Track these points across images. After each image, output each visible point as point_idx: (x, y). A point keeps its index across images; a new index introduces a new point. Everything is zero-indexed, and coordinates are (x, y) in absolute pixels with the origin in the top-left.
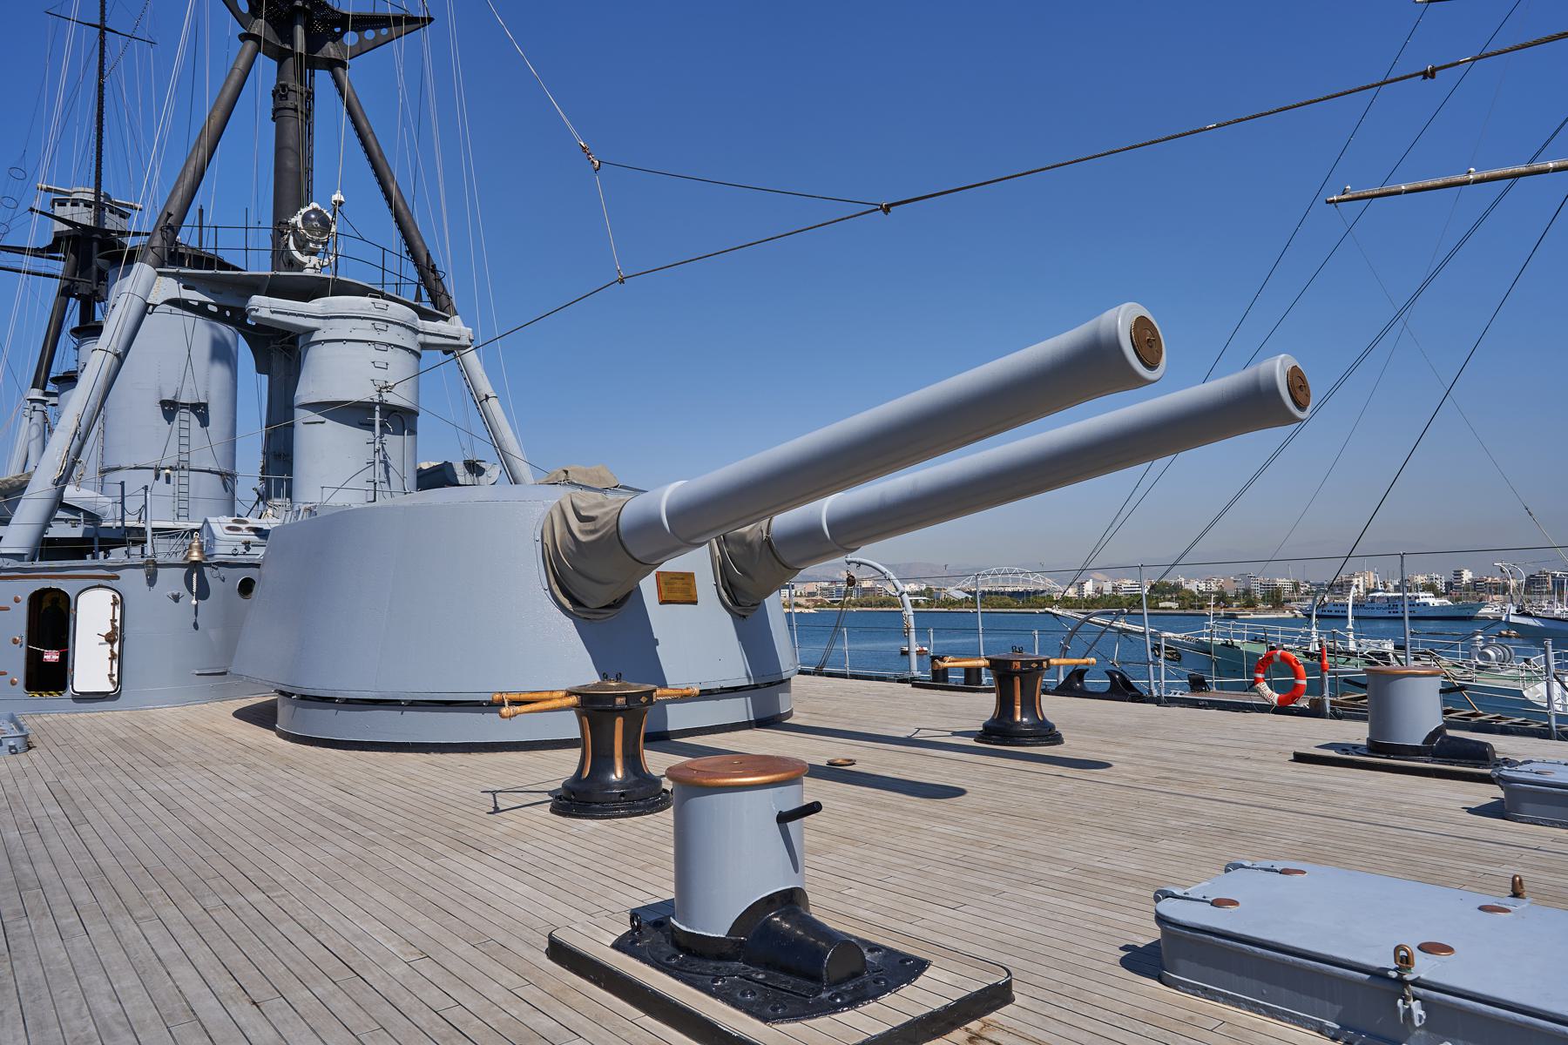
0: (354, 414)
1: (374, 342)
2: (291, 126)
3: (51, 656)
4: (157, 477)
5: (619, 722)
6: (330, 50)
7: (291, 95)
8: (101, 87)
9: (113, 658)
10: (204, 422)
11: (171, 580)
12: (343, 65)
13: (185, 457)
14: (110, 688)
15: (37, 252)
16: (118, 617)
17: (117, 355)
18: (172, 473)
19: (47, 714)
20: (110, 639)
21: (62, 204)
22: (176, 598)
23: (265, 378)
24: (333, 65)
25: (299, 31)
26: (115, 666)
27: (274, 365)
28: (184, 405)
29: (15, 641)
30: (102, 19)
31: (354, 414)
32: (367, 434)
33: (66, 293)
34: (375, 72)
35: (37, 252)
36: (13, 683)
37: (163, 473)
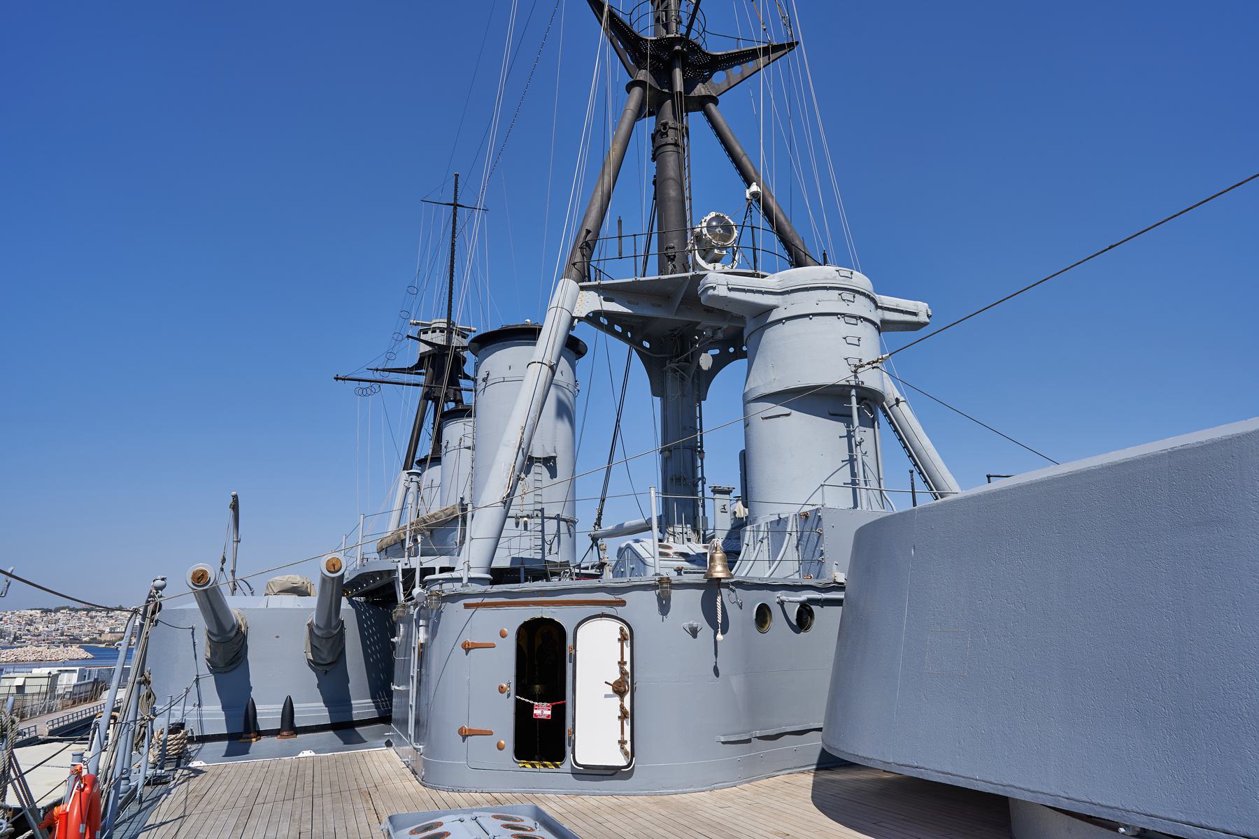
0: (826, 401)
1: (844, 315)
2: (671, 159)
3: (542, 711)
4: (517, 524)
6: (700, 90)
7: (671, 132)
8: (453, 245)
9: (624, 715)
10: (553, 474)
11: (687, 604)
14: (621, 761)
15: (409, 371)
16: (627, 658)
17: (551, 367)
19: (551, 792)
20: (619, 689)
21: (425, 333)
22: (694, 632)
23: (658, 400)
24: (702, 103)
25: (678, 73)
26: (627, 729)
27: (669, 384)
28: (538, 460)
29: (501, 690)
30: (455, 199)
31: (826, 401)
32: (840, 428)
33: (426, 397)
34: (744, 102)
35: (409, 371)
36: (500, 747)
37: (522, 521)
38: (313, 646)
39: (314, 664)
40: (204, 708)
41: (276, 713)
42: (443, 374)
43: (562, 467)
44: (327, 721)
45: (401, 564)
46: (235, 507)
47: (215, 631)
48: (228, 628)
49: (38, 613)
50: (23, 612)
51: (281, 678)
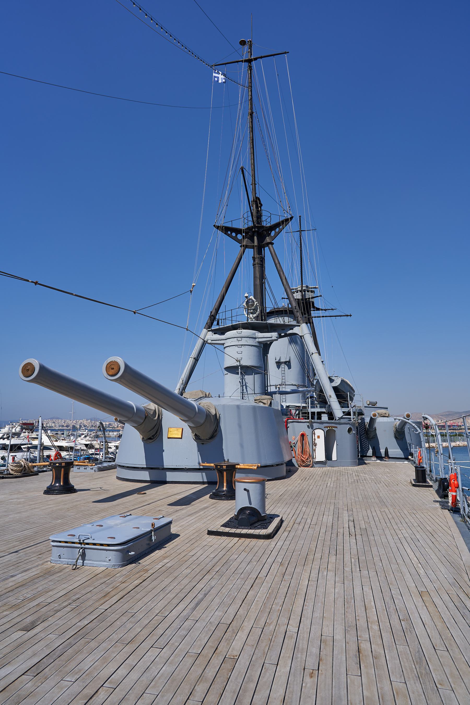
5: (63, 470)
10: (289, 367)
12: (272, 244)
13: (283, 381)
18: (280, 387)
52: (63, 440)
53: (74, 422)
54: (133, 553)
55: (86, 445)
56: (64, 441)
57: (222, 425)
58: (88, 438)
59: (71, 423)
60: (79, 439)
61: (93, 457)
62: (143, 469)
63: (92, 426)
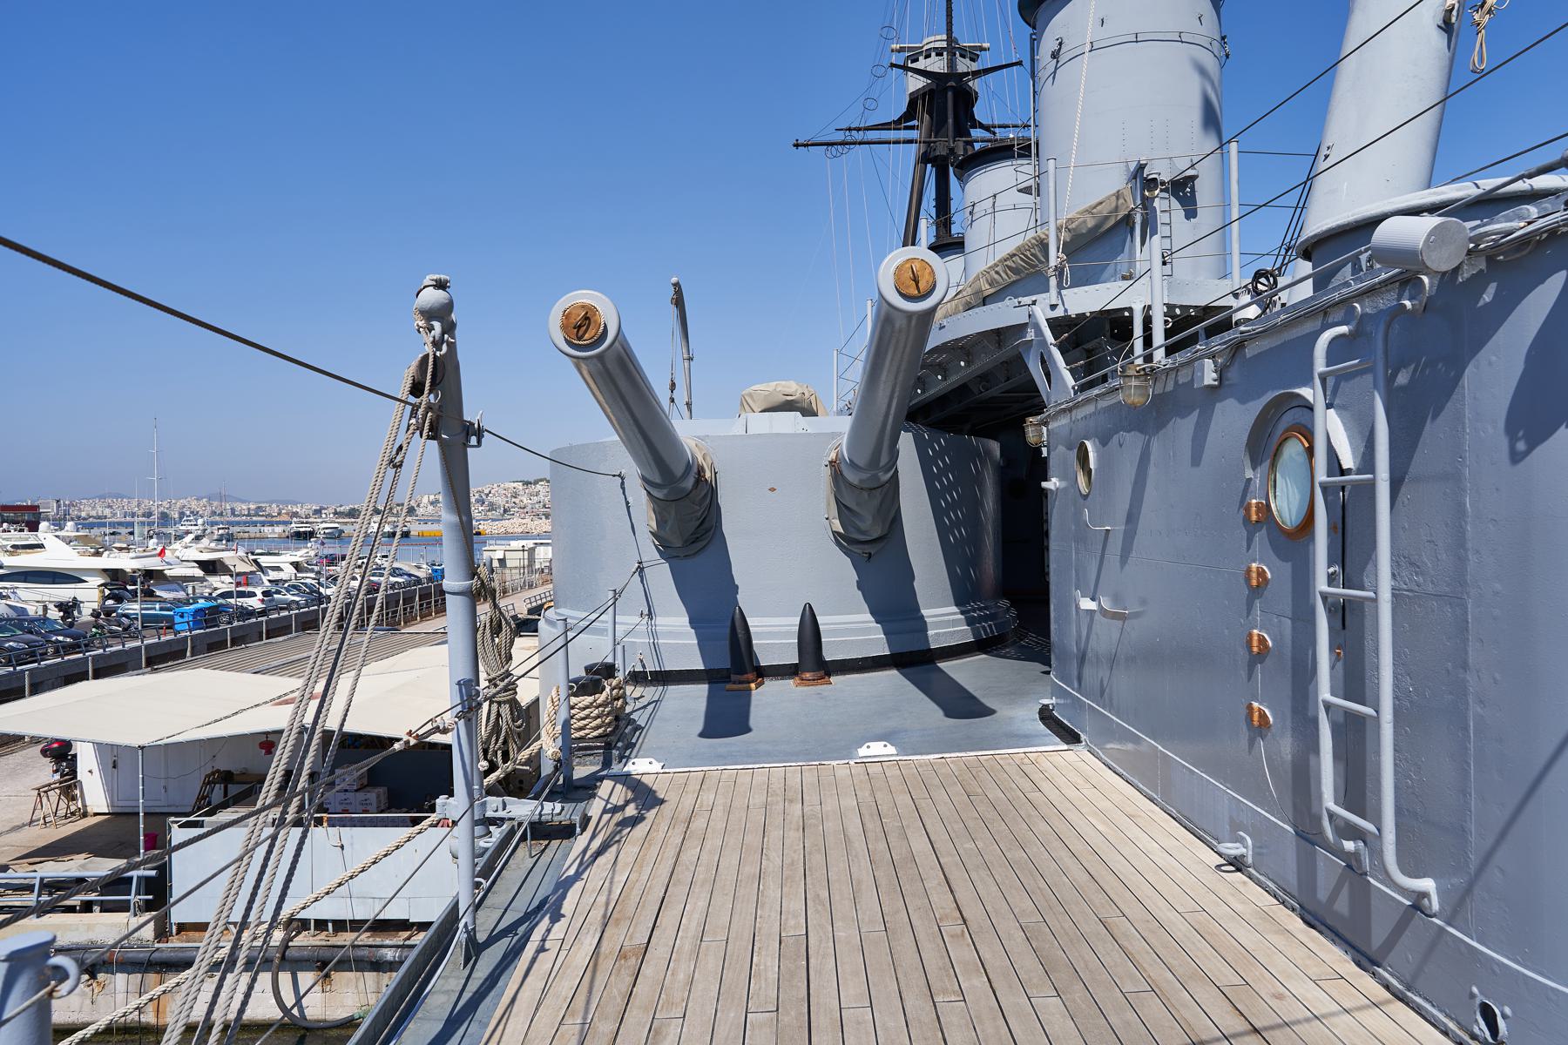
15: (896, 124)
33: (924, 159)
35: (896, 124)
38: (841, 506)
39: (846, 541)
40: (659, 620)
41: (786, 635)
42: (946, 121)
43: (1205, 193)
44: (884, 650)
45: (1042, 309)
46: (679, 302)
47: (658, 480)
48: (679, 471)
49: (519, 486)
50: (508, 485)
51: (788, 571)
52: (120, 549)
53: (165, 504)
54: (1487, 297)
55: (203, 565)
56: (124, 554)
57: (724, 500)
58: (205, 541)
59: (156, 506)
60: (177, 545)
61: (229, 606)
62: (342, 725)
63: (214, 513)
